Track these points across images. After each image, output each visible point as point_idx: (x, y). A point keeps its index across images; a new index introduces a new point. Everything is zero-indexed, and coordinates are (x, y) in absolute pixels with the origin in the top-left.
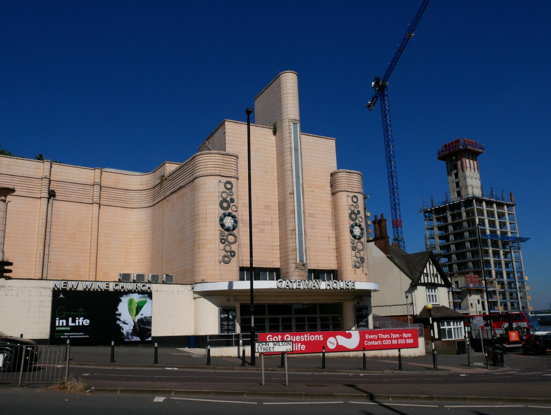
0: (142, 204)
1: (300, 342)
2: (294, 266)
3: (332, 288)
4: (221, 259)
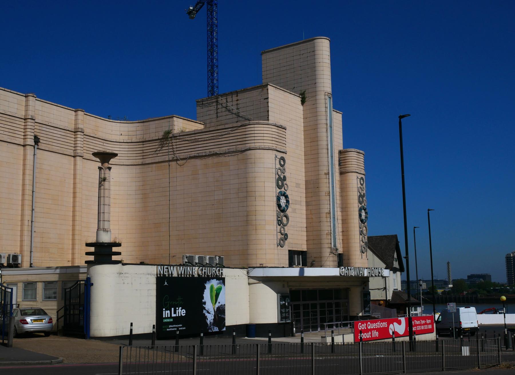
0: (123, 161)
2: (329, 250)
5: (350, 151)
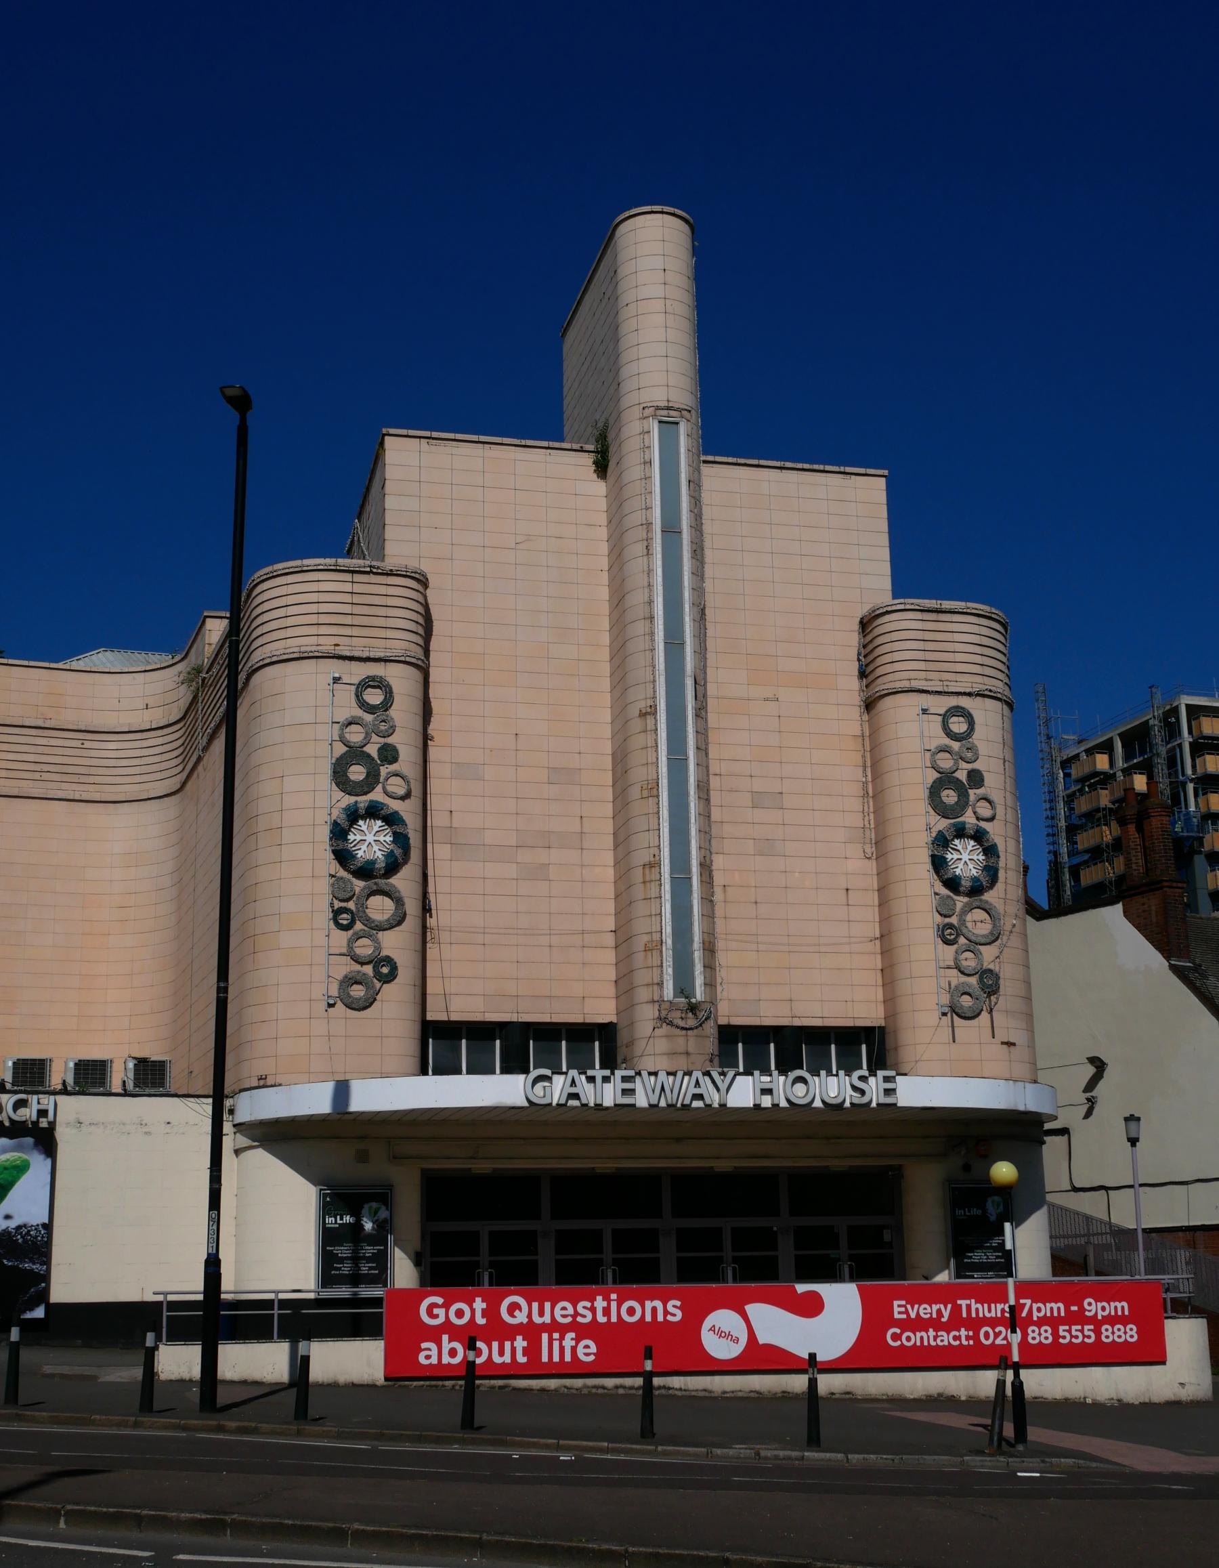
1: (574, 1326)
3: (783, 1104)
4: (334, 991)
5: (885, 610)
